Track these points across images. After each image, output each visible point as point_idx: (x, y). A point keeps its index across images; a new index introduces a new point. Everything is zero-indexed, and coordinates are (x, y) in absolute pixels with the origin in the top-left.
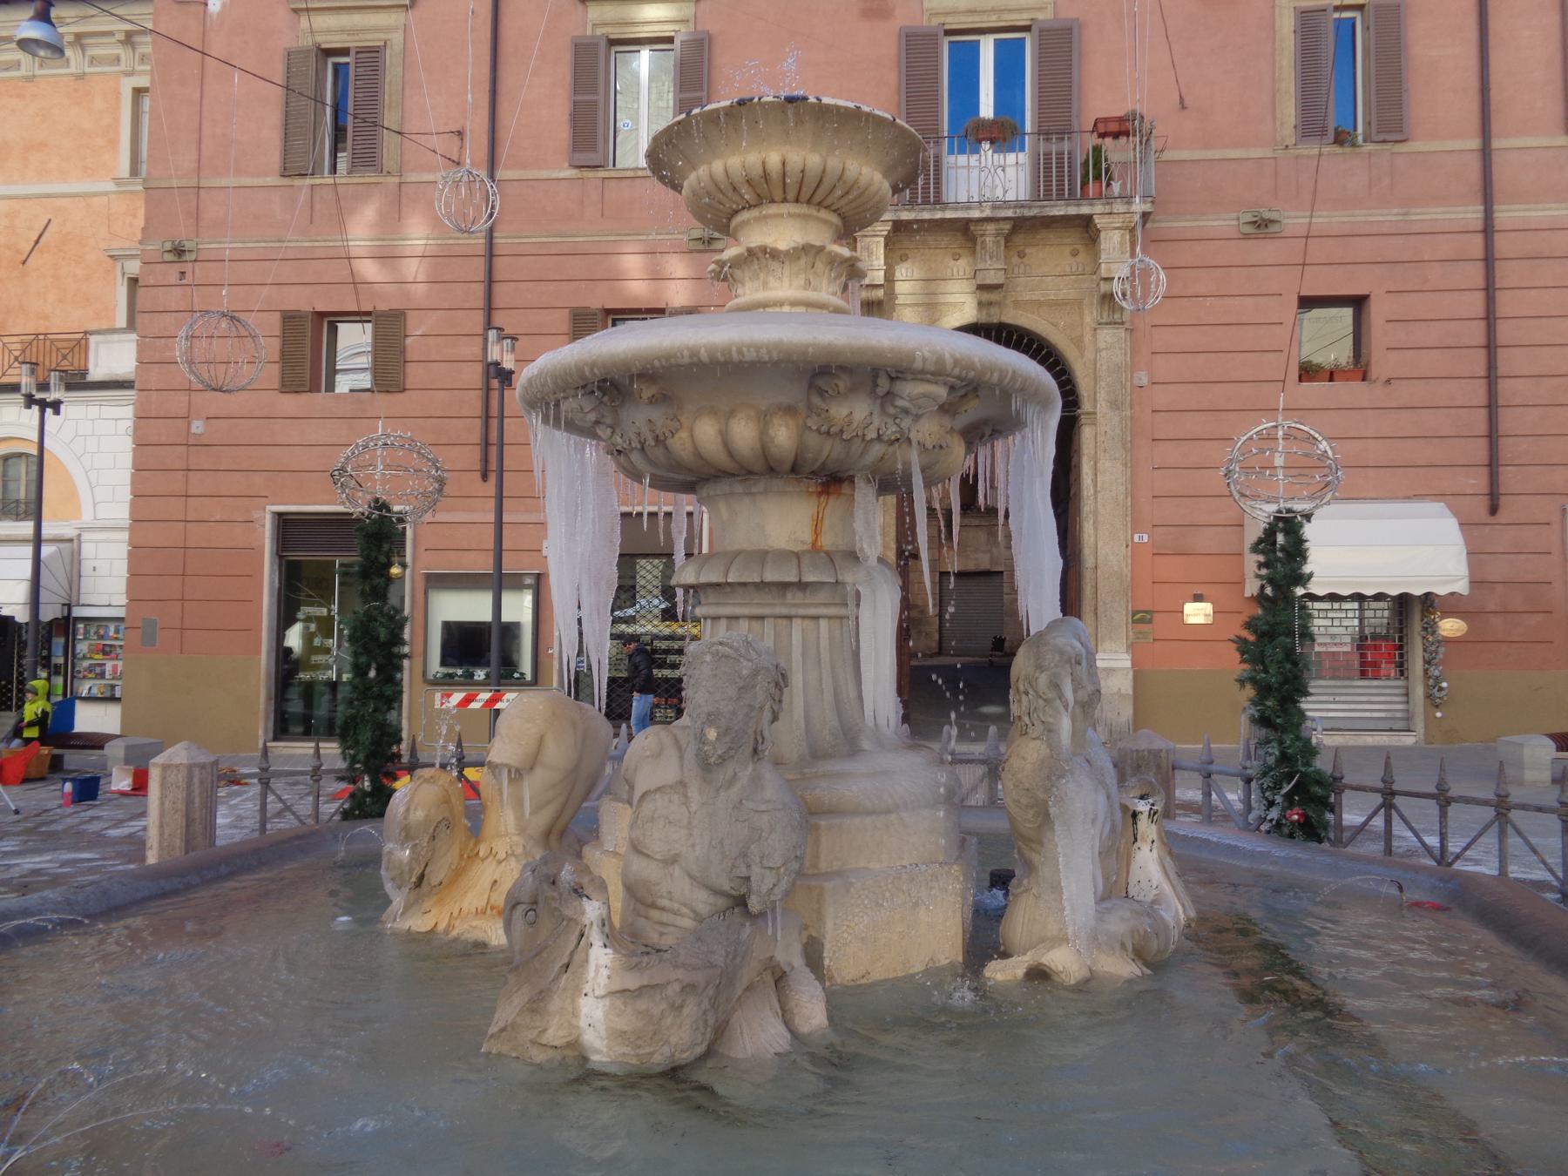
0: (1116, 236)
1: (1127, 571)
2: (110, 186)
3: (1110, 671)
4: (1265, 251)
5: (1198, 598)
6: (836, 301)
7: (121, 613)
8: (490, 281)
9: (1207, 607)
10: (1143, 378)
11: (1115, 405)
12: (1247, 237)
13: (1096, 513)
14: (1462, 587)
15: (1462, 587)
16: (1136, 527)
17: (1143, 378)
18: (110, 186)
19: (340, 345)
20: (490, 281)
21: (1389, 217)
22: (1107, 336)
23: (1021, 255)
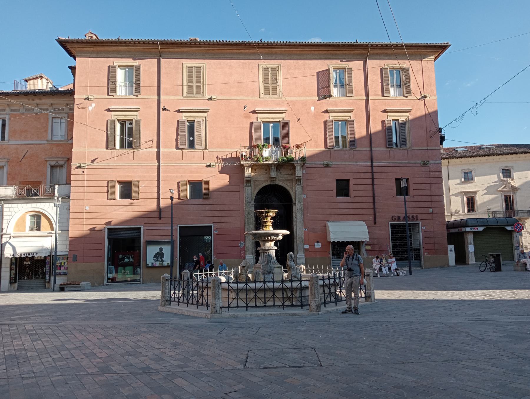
0: (299, 168)
1: (303, 237)
2: (46, 142)
3: (300, 258)
4: (329, 170)
5: (318, 242)
6: (65, 170)
7: (67, 253)
8: (374, 202)
9: (320, 244)
10: (305, 196)
11: (300, 202)
12: (325, 167)
13: (296, 224)
14: (368, 240)
15: (368, 240)
16: (305, 227)
17: (305, 196)
18: (46, 142)
19: (366, 130)
20: (374, 202)
21: (353, 163)
22: (297, 188)
23: (280, 170)
